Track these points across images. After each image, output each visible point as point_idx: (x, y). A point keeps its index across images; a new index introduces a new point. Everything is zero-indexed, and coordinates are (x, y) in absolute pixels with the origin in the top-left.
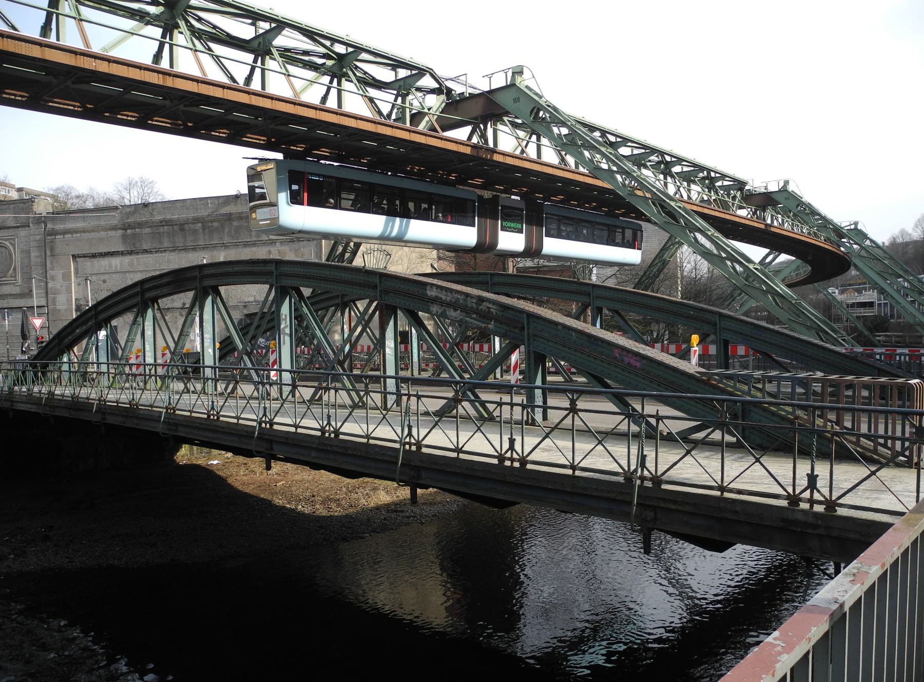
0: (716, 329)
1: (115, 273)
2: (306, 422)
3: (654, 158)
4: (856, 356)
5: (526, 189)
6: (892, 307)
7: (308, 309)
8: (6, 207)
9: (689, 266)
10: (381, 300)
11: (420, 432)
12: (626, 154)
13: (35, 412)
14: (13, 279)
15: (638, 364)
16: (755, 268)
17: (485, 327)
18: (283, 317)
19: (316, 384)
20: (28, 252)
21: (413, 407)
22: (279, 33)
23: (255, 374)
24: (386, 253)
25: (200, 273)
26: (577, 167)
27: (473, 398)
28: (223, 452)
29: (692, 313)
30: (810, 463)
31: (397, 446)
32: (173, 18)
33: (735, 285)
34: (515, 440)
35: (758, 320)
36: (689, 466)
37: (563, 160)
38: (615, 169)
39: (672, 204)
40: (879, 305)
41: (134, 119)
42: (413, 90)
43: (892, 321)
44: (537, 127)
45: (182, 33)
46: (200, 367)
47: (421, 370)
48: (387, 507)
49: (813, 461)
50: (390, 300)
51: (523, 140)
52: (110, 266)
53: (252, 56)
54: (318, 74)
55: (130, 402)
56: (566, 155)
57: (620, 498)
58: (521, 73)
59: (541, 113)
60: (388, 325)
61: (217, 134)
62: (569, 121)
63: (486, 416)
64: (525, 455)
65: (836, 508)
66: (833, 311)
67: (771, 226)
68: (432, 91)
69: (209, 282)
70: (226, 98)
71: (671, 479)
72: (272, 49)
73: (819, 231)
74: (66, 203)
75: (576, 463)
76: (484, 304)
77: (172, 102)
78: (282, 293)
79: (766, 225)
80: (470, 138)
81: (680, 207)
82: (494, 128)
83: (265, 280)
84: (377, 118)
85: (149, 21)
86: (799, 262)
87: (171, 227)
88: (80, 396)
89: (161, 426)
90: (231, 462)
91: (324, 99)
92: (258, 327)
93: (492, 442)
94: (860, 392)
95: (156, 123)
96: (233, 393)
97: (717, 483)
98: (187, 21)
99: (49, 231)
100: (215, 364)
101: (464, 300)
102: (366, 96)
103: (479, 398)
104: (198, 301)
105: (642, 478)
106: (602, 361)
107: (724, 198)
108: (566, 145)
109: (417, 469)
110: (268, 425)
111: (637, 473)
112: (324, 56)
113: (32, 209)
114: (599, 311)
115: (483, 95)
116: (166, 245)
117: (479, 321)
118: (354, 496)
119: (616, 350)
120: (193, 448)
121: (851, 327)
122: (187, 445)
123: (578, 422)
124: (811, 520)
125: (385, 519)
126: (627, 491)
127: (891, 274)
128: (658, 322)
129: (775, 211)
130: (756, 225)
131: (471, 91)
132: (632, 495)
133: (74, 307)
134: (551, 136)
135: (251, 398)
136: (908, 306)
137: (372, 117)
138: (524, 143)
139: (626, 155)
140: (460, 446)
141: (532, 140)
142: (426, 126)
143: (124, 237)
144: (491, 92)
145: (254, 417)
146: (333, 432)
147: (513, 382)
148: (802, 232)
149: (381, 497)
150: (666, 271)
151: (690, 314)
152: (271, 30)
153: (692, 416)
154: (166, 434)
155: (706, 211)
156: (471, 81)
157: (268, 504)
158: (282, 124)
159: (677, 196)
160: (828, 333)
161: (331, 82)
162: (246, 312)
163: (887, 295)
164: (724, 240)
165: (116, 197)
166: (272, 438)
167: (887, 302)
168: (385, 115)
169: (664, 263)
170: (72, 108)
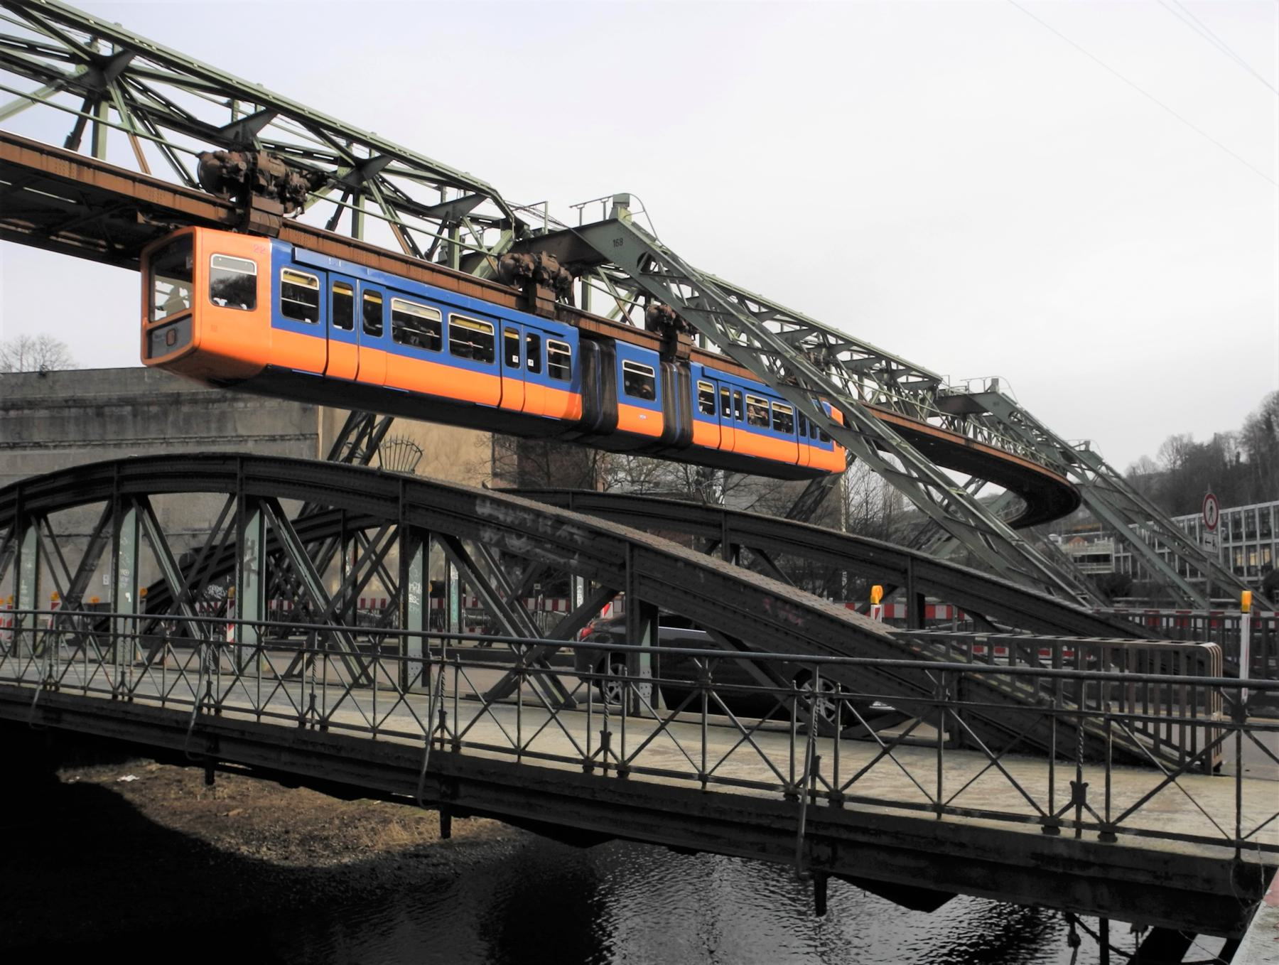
3: (811, 338)
4: (1108, 619)
6: (1134, 561)
15: (800, 621)
18: (249, 543)
22: (268, 122)
24: (415, 448)
25: (119, 472)
31: (421, 744)
34: (610, 734)
36: (881, 775)
38: (757, 344)
40: (1118, 559)
41: (27, 232)
43: (1135, 581)
45: (115, 108)
46: (108, 618)
50: (419, 520)
57: (777, 825)
58: (625, 204)
60: (413, 557)
63: (562, 700)
67: (974, 441)
68: (495, 224)
69: (130, 488)
75: (708, 771)
76: (564, 527)
78: (250, 505)
79: (968, 440)
82: (583, 283)
84: (410, 256)
86: (1011, 495)
87: (82, 411)
90: (156, 778)
91: (333, 224)
95: (63, 240)
98: (124, 91)
102: (396, 223)
104: (112, 518)
105: (814, 794)
111: (805, 784)
112: (336, 161)
115: (568, 232)
116: (71, 437)
119: (767, 600)
124: (1078, 855)
125: (399, 868)
126: (788, 815)
127: (1137, 513)
131: (551, 226)
136: (1160, 564)
140: (523, 745)
144: (582, 229)
146: (318, 722)
148: (1015, 451)
149: (394, 834)
150: (825, 503)
152: (257, 115)
154: (41, 726)
156: (552, 213)
161: (344, 198)
163: (1129, 545)
166: (217, 731)
168: (423, 253)
169: (822, 492)
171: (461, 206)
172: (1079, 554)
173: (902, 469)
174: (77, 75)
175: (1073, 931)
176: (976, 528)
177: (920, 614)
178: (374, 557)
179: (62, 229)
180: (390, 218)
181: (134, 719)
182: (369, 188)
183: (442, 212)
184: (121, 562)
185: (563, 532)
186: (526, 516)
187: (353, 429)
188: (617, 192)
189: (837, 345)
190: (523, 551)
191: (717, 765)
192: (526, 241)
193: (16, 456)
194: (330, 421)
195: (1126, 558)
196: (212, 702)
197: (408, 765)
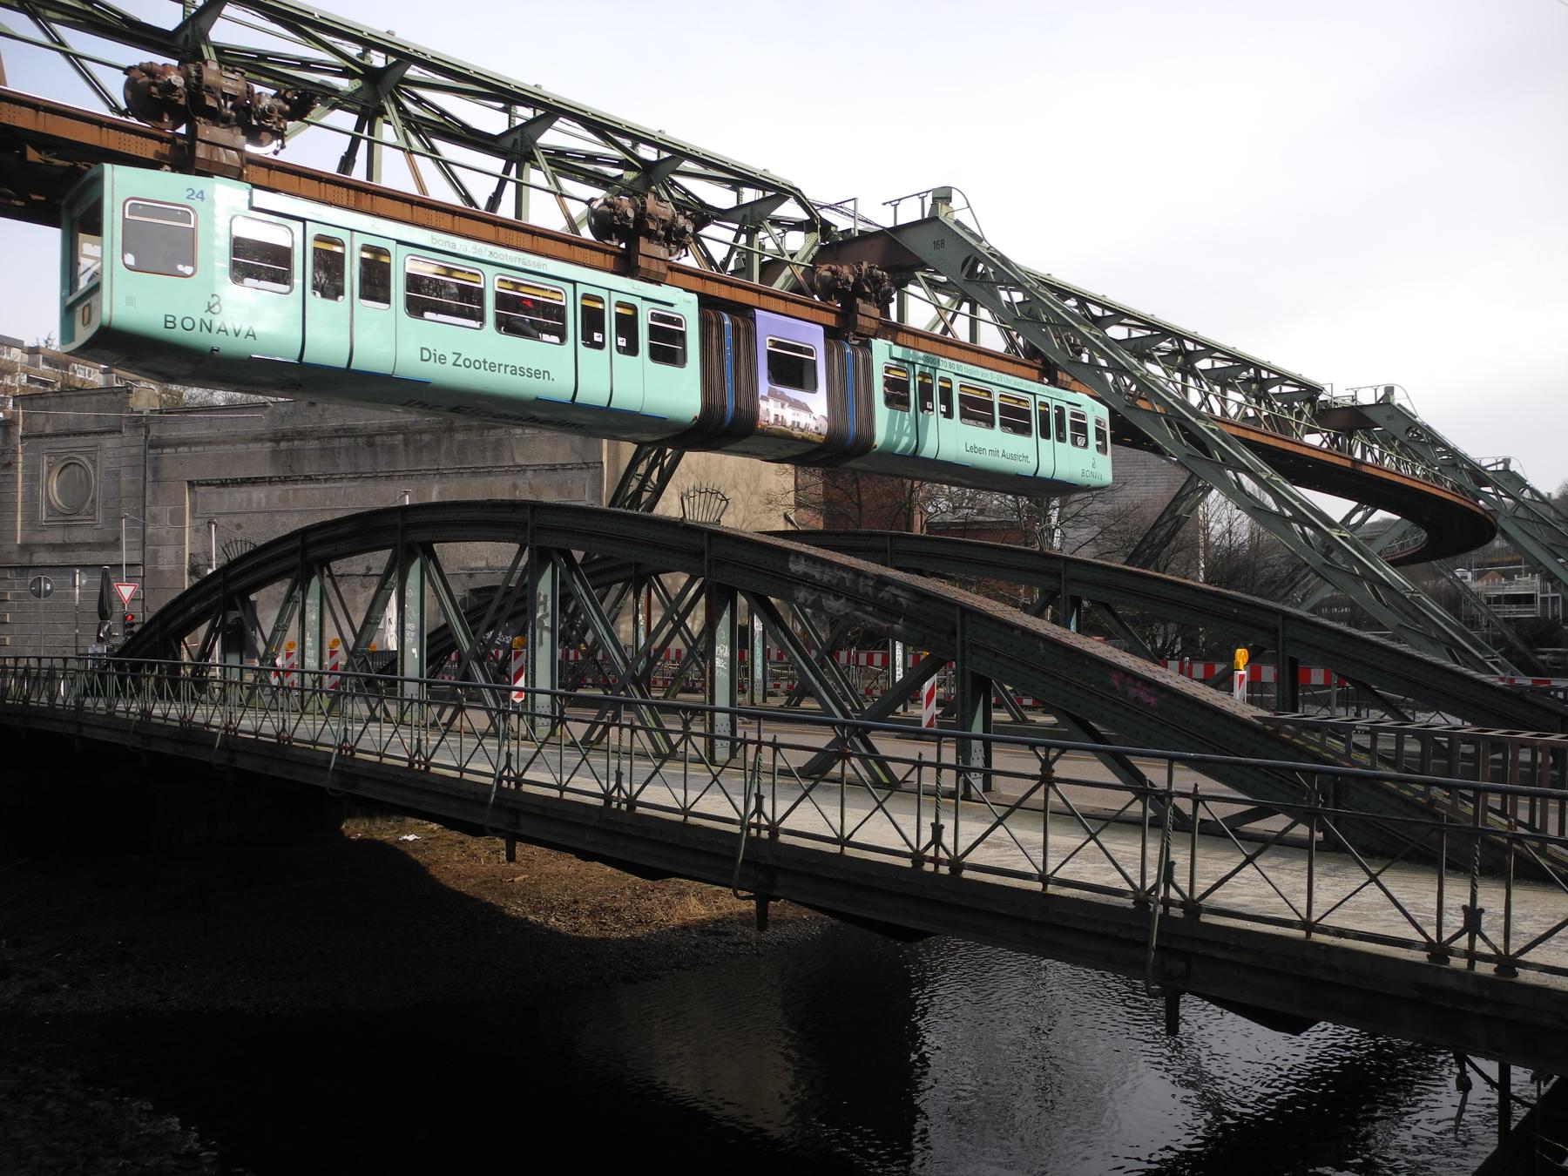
1: (257, 512)
3: (1165, 344)
7: (585, 587)
8: (85, 399)
9: (1218, 527)
11: (778, 806)
12: (1119, 338)
14: (90, 517)
15: (1153, 700)
16: (1341, 537)
17: (888, 628)
18: (542, 598)
20: (117, 474)
22: (549, 126)
23: (489, 694)
24: (720, 497)
27: (864, 751)
29: (1235, 611)
30: (1469, 884)
31: (736, 829)
32: (377, 98)
34: (942, 827)
35: (1333, 620)
36: (1243, 881)
38: (1103, 363)
39: (1201, 425)
40: (1544, 600)
42: (767, 223)
44: (972, 290)
45: (389, 123)
46: (396, 680)
47: (766, 694)
48: (703, 928)
49: (1474, 886)
52: (250, 501)
55: (278, 734)
58: (948, 199)
59: (980, 268)
60: (720, 618)
63: (885, 780)
64: (959, 854)
65: (1517, 969)
66: (1464, 609)
67: (1362, 462)
68: (798, 226)
69: (417, 536)
72: (535, 151)
76: (887, 589)
78: (541, 557)
79: (1355, 461)
81: (1213, 430)
83: (513, 535)
85: (337, 103)
86: (1407, 524)
90: (438, 838)
92: (500, 609)
93: (900, 826)
94: (1515, 756)
96: (598, 743)
97: (1299, 915)
98: (399, 104)
100: (421, 675)
101: (853, 581)
104: (398, 568)
105: (1167, 902)
110: (513, 784)
112: (620, 164)
113: (127, 403)
114: (1076, 602)
115: (884, 233)
116: (342, 469)
117: (879, 618)
118: (645, 904)
119: (1115, 676)
121: (1494, 637)
123: (1054, 799)
125: (697, 946)
126: (1138, 925)
128: (1164, 621)
129: (1369, 438)
130: (1336, 461)
131: (861, 226)
132: (1149, 931)
133: (187, 567)
135: (485, 734)
137: (698, 267)
138: (950, 315)
139: (1119, 338)
141: (962, 310)
142: (785, 284)
143: (275, 454)
144: (897, 229)
145: (490, 770)
146: (625, 801)
148: (1414, 473)
150: (1180, 534)
151: (1233, 612)
155: (1253, 436)
156: (863, 211)
157: (493, 915)
159: (1204, 409)
160: (1467, 651)
162: (472, 585)
163: (1559, 584)
164: (1288, 486)
167: (1557, 595)
168: (718, 263)
169: (1177, 522)
171: (758, 208)
173: (1274, 508)
174: (350, 90)
175: (1463, 1073)
176: (1362, 578)
177: (1292, 678)
184: (407, 615)
186: (845, 575)
188: (936, 186)
189: (1195, 351)
190: (841, 613)
192: (833, 245)
194: (615, 457)
195: (1555, 599)
196: (512, 775)
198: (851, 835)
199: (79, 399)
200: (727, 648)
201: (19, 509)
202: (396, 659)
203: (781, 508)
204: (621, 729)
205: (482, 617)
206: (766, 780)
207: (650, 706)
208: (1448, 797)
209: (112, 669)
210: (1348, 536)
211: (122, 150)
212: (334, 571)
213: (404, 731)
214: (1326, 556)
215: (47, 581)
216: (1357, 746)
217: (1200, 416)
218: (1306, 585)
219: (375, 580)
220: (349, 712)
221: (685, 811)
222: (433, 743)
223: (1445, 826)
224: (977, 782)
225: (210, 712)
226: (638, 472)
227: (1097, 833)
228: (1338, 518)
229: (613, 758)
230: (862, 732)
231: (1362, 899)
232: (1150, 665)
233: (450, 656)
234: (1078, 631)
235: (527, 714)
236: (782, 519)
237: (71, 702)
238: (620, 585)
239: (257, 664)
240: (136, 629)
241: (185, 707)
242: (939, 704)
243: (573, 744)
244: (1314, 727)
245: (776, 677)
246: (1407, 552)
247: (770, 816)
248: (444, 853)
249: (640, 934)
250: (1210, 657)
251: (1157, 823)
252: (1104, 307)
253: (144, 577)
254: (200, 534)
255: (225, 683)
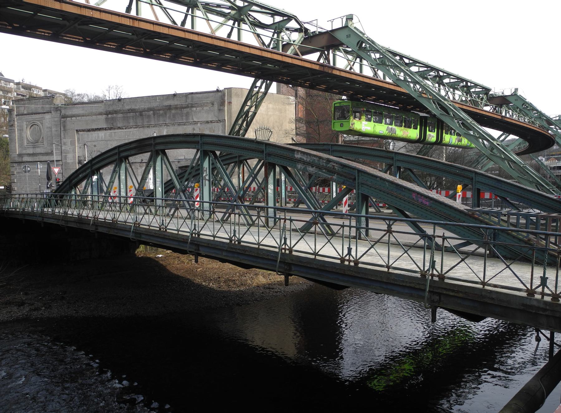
0: (472, 182)
1: (101, 141)
2: (220, 234)
3: (432, 73)
5: (352, 92)
8: (38, 101)
10: (266, 160)
13: (56, 224)
15: (428, 203)
17: (331, 178)
18: (205, 169)
19: (224, 210)
20: (51, 128)
21: (288, 226)
23: (187, 204)
24: (269, 130)
25: (154, 142)
26: (384, 78)
27: (322, 222)
28: (165, 250)
30: (543, 269)
31: (277, 250)
33: (484, 154)
34: (351, 249)
36: (460, 268)
37: (376, 74)
38: (410, 80)
39: (446, 103)
41: (114, 47)
44: (361, 53)
47: (286, 203)
50: (271, 160)
51: (352, 61)
52: (98, 137)
53: (186, 8)
54: (226, 20)
55: (113, 219)
56: (377, 70)
58: (352, 19)
59: (364, 45)
60: (270, 175)
61: (164, 56)
62: (381, 49)
63: (330, 233)
64: (357, 258)
65: (559, 299)
67: (505, 117)
68: (296, 30)
70: (170, 34)
71: (449, 276)
72: (198, 3)
73: (535, 121)
74: (72, 99)
75: (390, 264)
76: (331, 163)
77: (137, 36)
78: (205, 154)
79: (502, 116)
80: (319, 60)
81: (450, 105)
83: (194, 146)
84: (262, 47)
86: (521, 140)
87: (134, 114)
88: (83, 215)
89: (131, 234)
90: (170, 256)
91: (229, 35)
92: (190, 174)
93: (336, 249)
95: (127, 49)
96: (227, 221)
97: (480, 280)
99: (62, 115)
100: (162, 197)
102: (255, 33)
103: (326, 222)
104: (153, 159)
105: (433, 275)
106: (405, 201)
107: (476, 99)
108: (377, 65)
109: (289, 265)
110: (197, 235)
111: (429, 272)
112: (230, 8)
113: (53, 102)
114: (399, 168)
115: (327, 32)
116: (131, 124)
118: (244, 278)
119: (414, 194)
120: (147, 247)
122: (143, 245)
123: (392, 239)
124: (542, 306)
125: (263, 293)
126: (422, 283)
128: (430, 175)
129: (508, 108)
130: (495, 116)
131: (320, 30)
132: (426, 285)
133: (77, 161)
134: (369, 59)
135: (186, 218)
140: (317, 251)
141: (357, 61)
143: (107, 119)
144: (333, 31)
146: (237, 241)
147: (344, 212)
148: (524, 121)
151: (456, 172)
153: (462, 236)
155: (464, 107)
156: (320, 24)
158: (204, 50)
160: (543, 186)
164: (480, 127)
165: (101, 95)
166: (199, 243)
168: (267, 45)
170: (78, 40)
171: (281, 24)
172: (553, 166)
175: (538, 336)
177: (478, 194)
178: (253, 176)
179: (127, 45)
180: (253, 31)
181: (168, 238)
182: (244, 19)
183: (274, 26)
185: (330, 165)
187: (240, 118)
190: (314, 172)
191: (395, 261)
193: (112, 132)
196: (196, 232)
197: (272, 258)
198: (318, 252)
199: (36, 101)
200: (272, 186)
201: (17, 141)
202: (153, 192)
203: (291, 135)
204: (235, 215)
205: (184, 177)
206: (288, 233)
207: (245, 206)
208: (535, 238)
209: (53, 198)
210: (500, 144)
211: (46, 6)
212: (131, 162)
213: (156, 217)
214: (491, 151)
215: (28, 167)
216: (502, 220)
217: (445, 100)
218: (483, 163)
219: (144, 164)
220: (138, 211)
221: (259, 244)
222: (168, 221)
223: (535, 248)
224: (363, 231)
225: (88, 212)
226: (238, 123)
227: (408, 250)
228: (496, 137)
229: (232, 226)
230: (322, 215)
231: (503, 274)
232: (427, 190)
233: (172, 191)
234: (400, 178)
235: (201, 210)
236: (291, 140)
237: (39, 209)
238: (233, 164)
239: (103, 194)
240: (60, 183)
241: (79, 210)
242: (349, 206)
243: (218, 221)
244: (487, 213)
245: (289, 197)
246: (521, 150)
247: (289, 245)
248: (172, 261)
249: (242, 289)
250: (448, 189)
251: (429, 248)
252: (409, 59)
253: (62, 165)
254: (81, 149)
255: (93, 202)
